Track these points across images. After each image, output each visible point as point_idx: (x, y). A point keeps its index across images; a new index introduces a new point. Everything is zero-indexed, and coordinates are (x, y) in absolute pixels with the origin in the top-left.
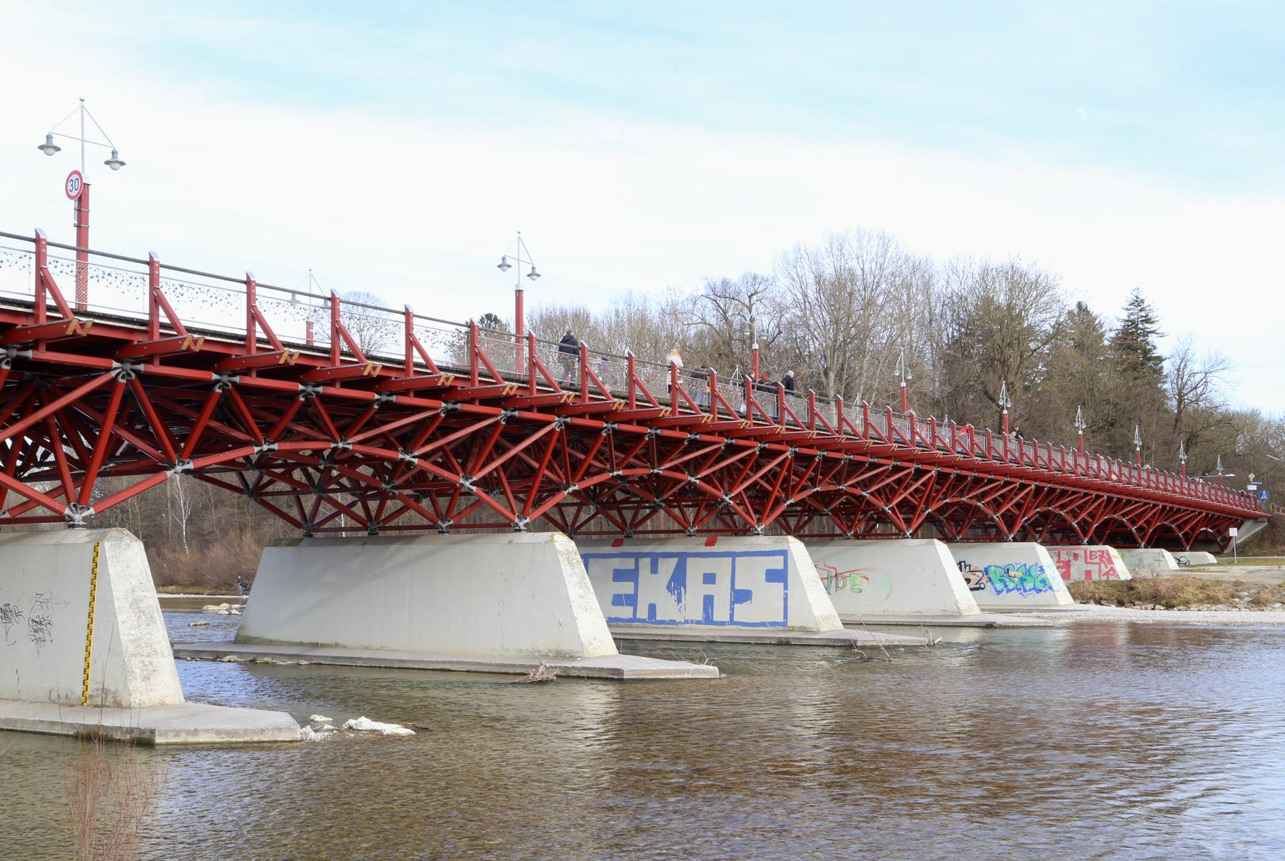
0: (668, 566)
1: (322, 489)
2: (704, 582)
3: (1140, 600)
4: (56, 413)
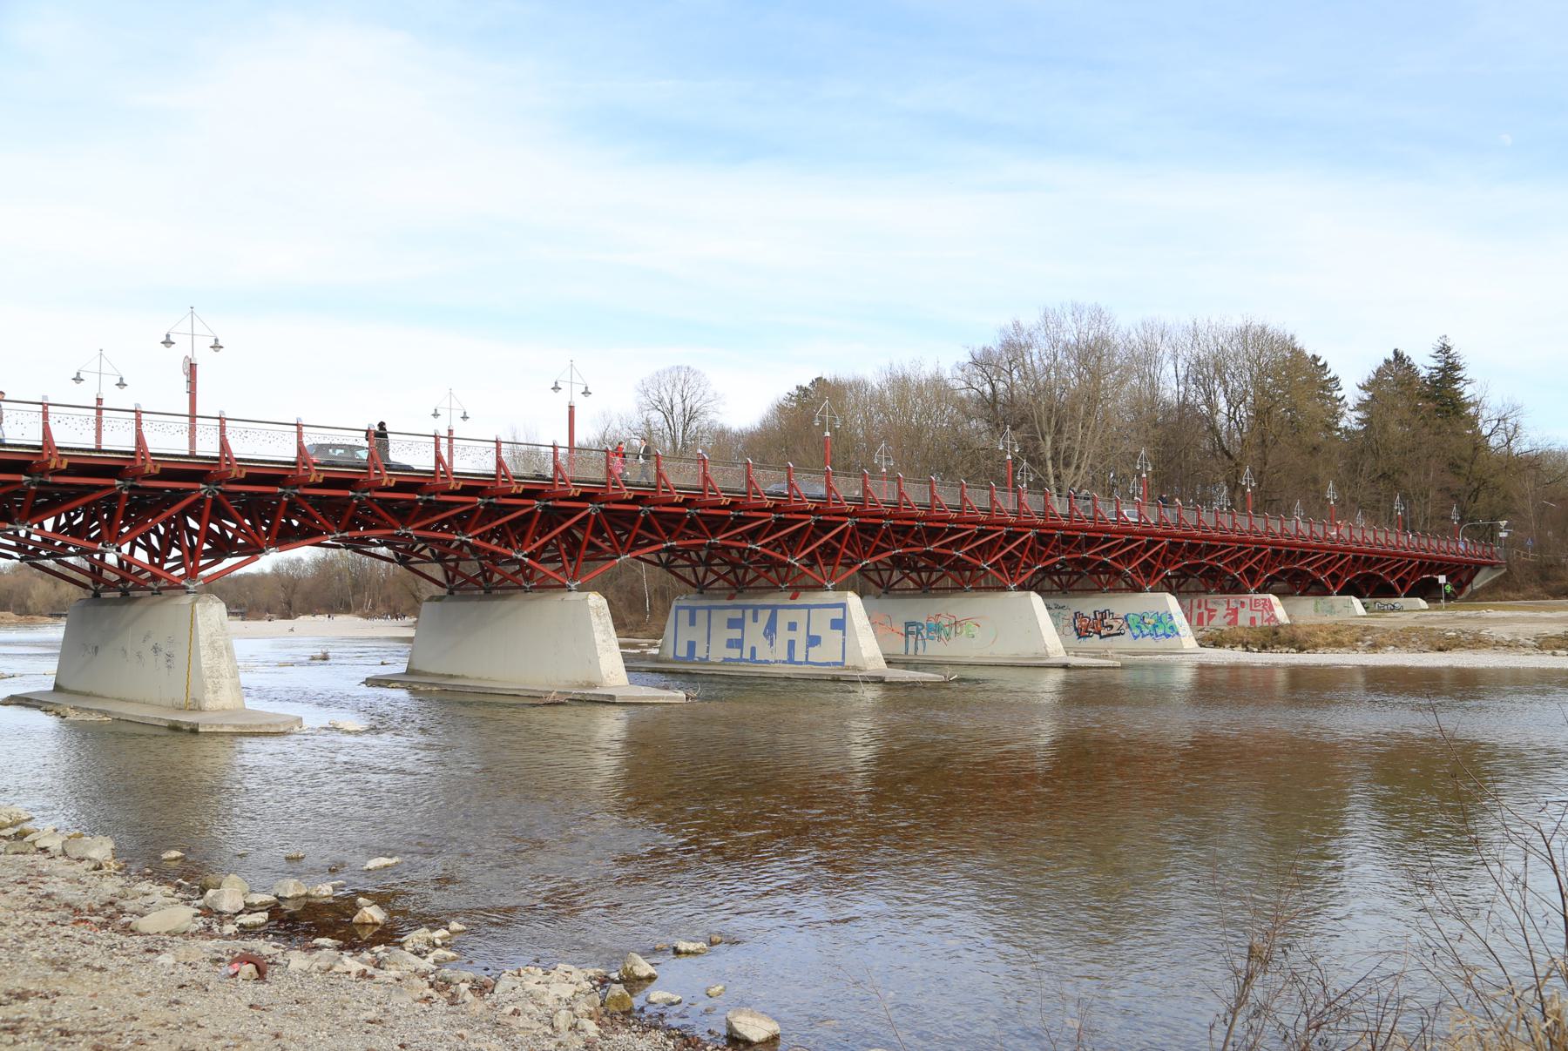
0: (764, 616)
1: (707, 563)
2: (832, 628)
3: (1279, 644)
4: (561, 533)
